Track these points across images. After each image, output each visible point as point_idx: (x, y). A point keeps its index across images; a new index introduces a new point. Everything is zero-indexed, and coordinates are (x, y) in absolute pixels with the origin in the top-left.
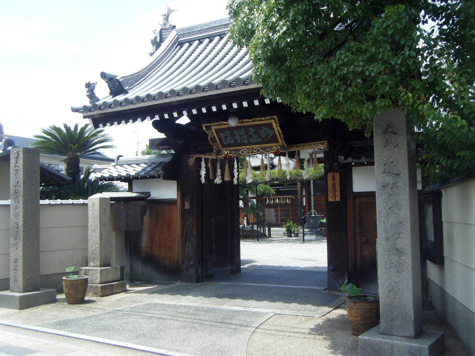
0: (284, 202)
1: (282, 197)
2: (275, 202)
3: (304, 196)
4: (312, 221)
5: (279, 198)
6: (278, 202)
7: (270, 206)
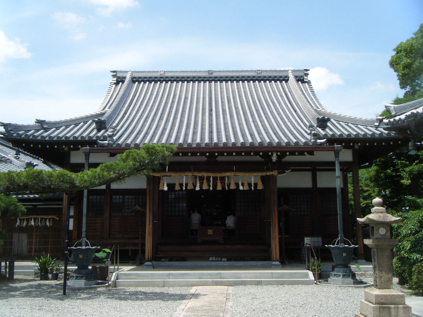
0: (43, 224)
1: (40, 217)
2: (29, 225)
3: (72, 217)
4: (81, 256)
5: (35, 219)
6: (33, 223)
7: (21, 230)
